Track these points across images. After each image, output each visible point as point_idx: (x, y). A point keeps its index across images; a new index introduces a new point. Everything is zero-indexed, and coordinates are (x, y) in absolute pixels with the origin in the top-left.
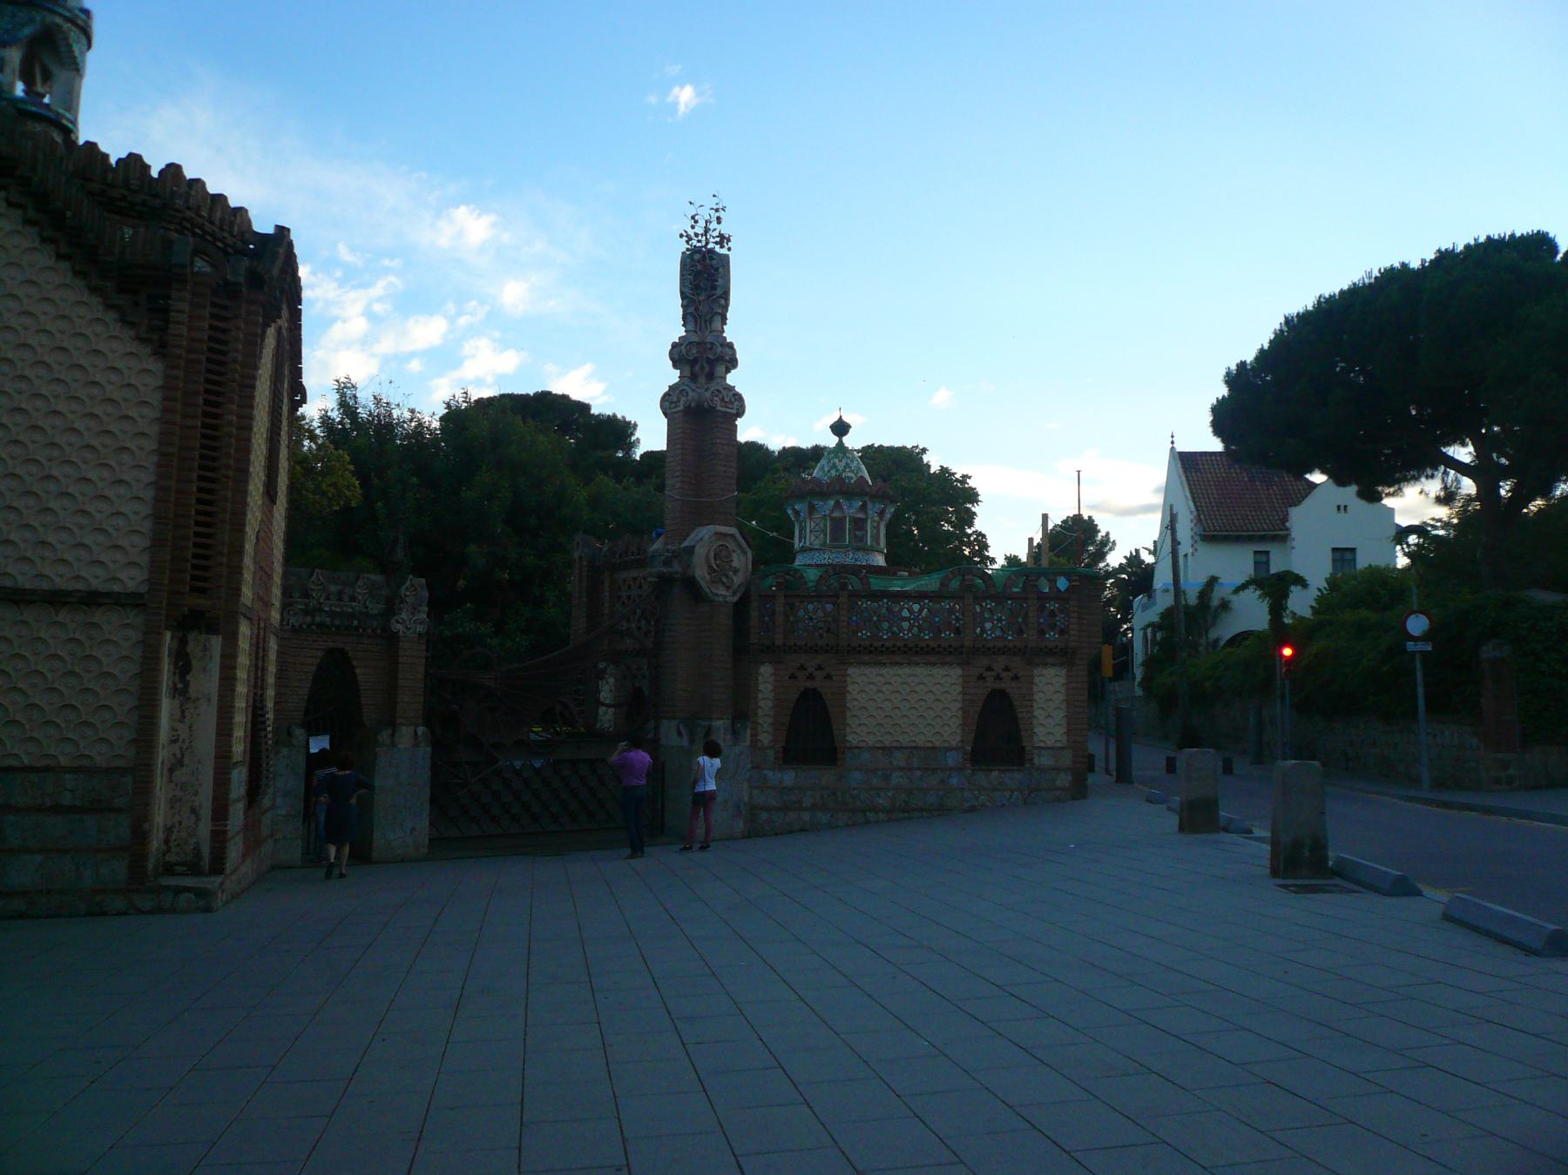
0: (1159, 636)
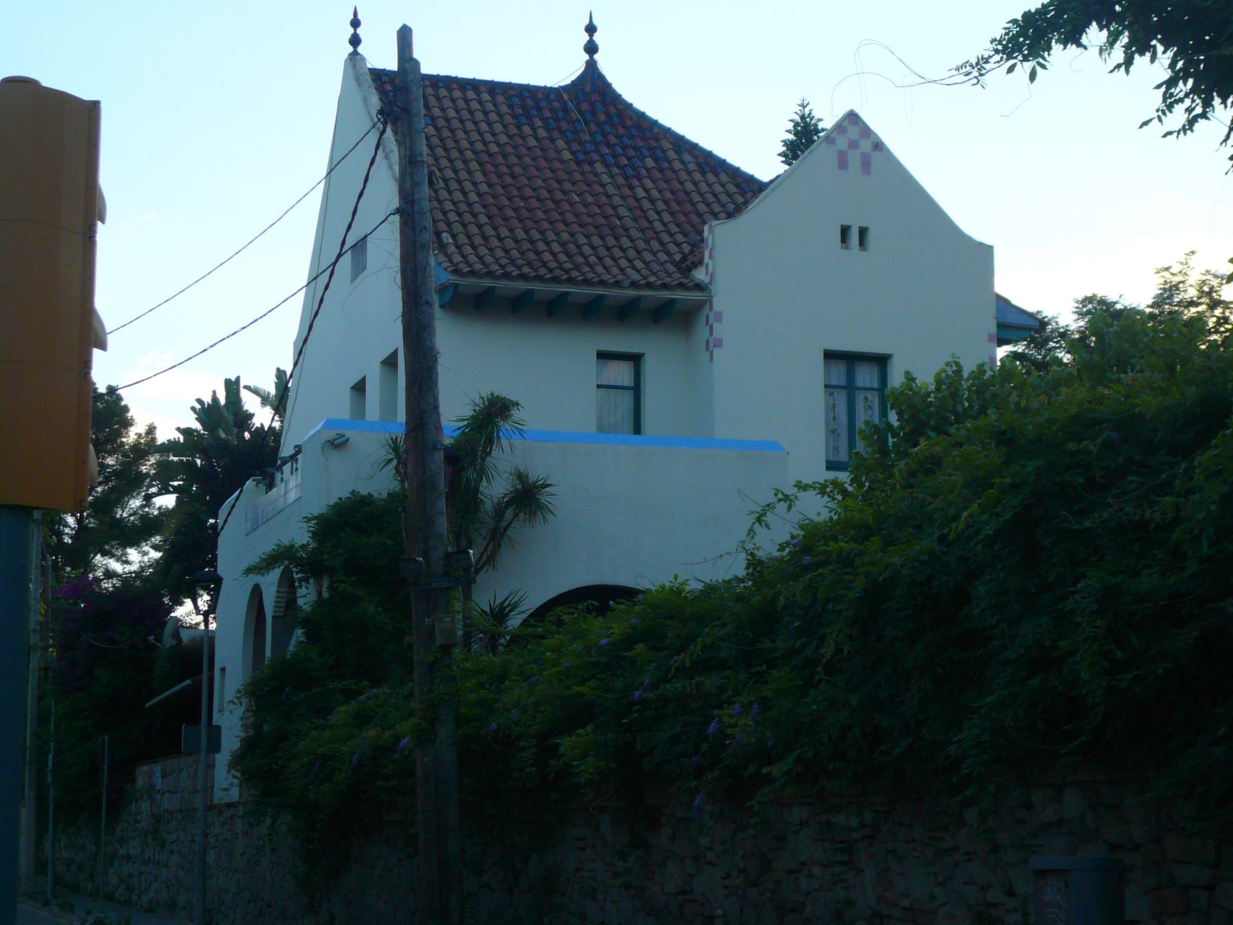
0: (306, 597)
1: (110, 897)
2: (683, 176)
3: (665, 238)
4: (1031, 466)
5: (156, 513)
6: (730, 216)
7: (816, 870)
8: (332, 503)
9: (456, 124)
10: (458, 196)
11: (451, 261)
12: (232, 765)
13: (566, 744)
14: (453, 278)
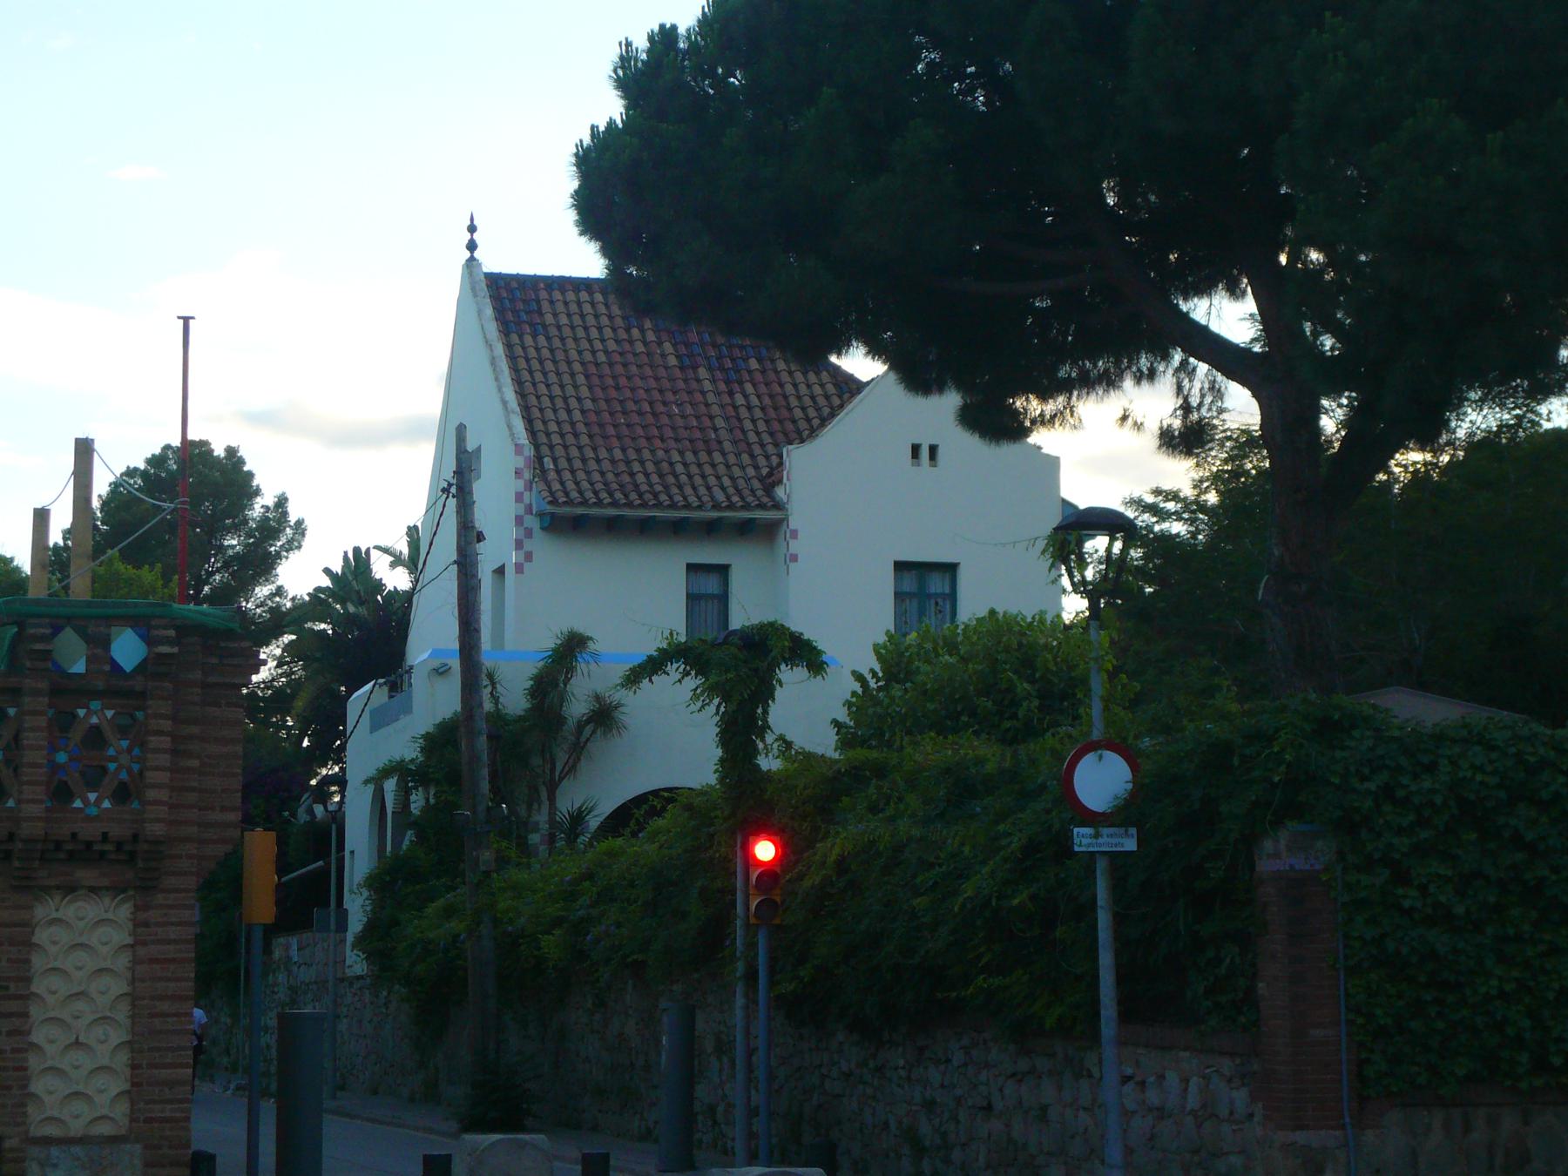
0: (417, 801)
3: (757, 450)
5: (289, 605)
6: (802, 441)
8: (437, 722)
10: (563, 415)
11: (550, 491)
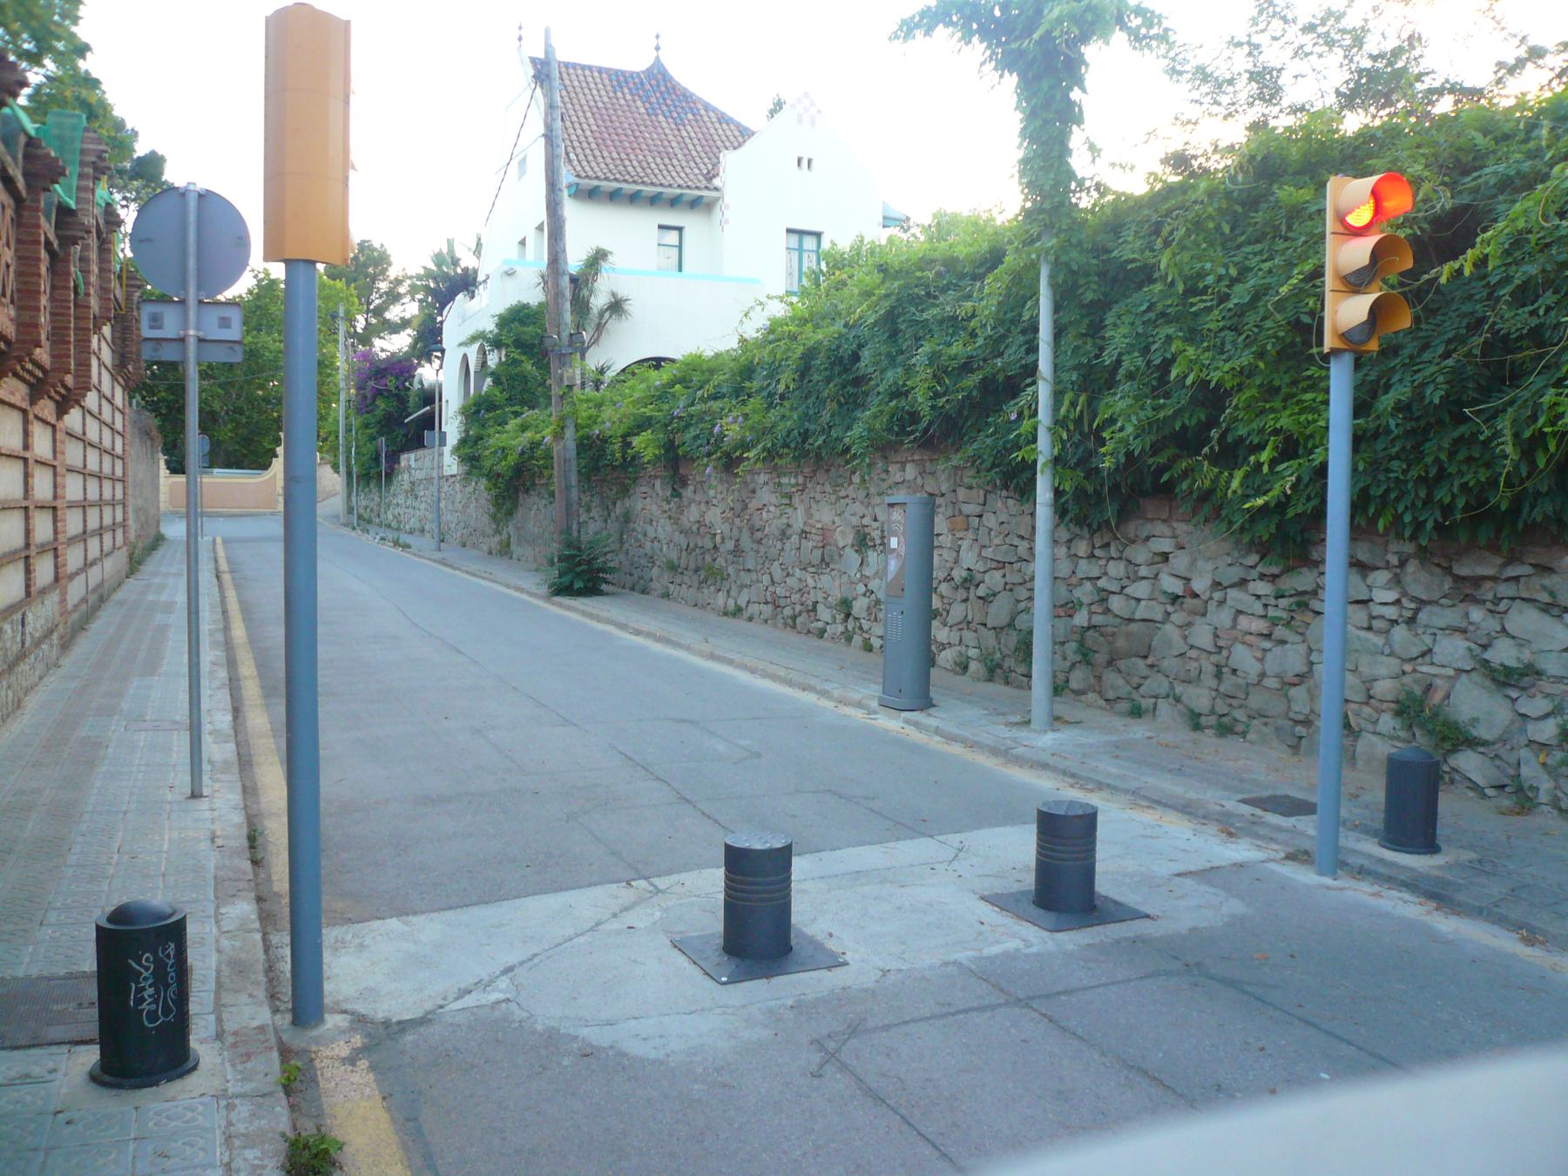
0: (493, 360)
1: (389, 526)
2: (709, 125)
4: (896, 284)
7: (772, 509)
9: (578, 90)
10: (579, 132)
12: (453, 453)
13: (637, 441)
14: (577, 180)
